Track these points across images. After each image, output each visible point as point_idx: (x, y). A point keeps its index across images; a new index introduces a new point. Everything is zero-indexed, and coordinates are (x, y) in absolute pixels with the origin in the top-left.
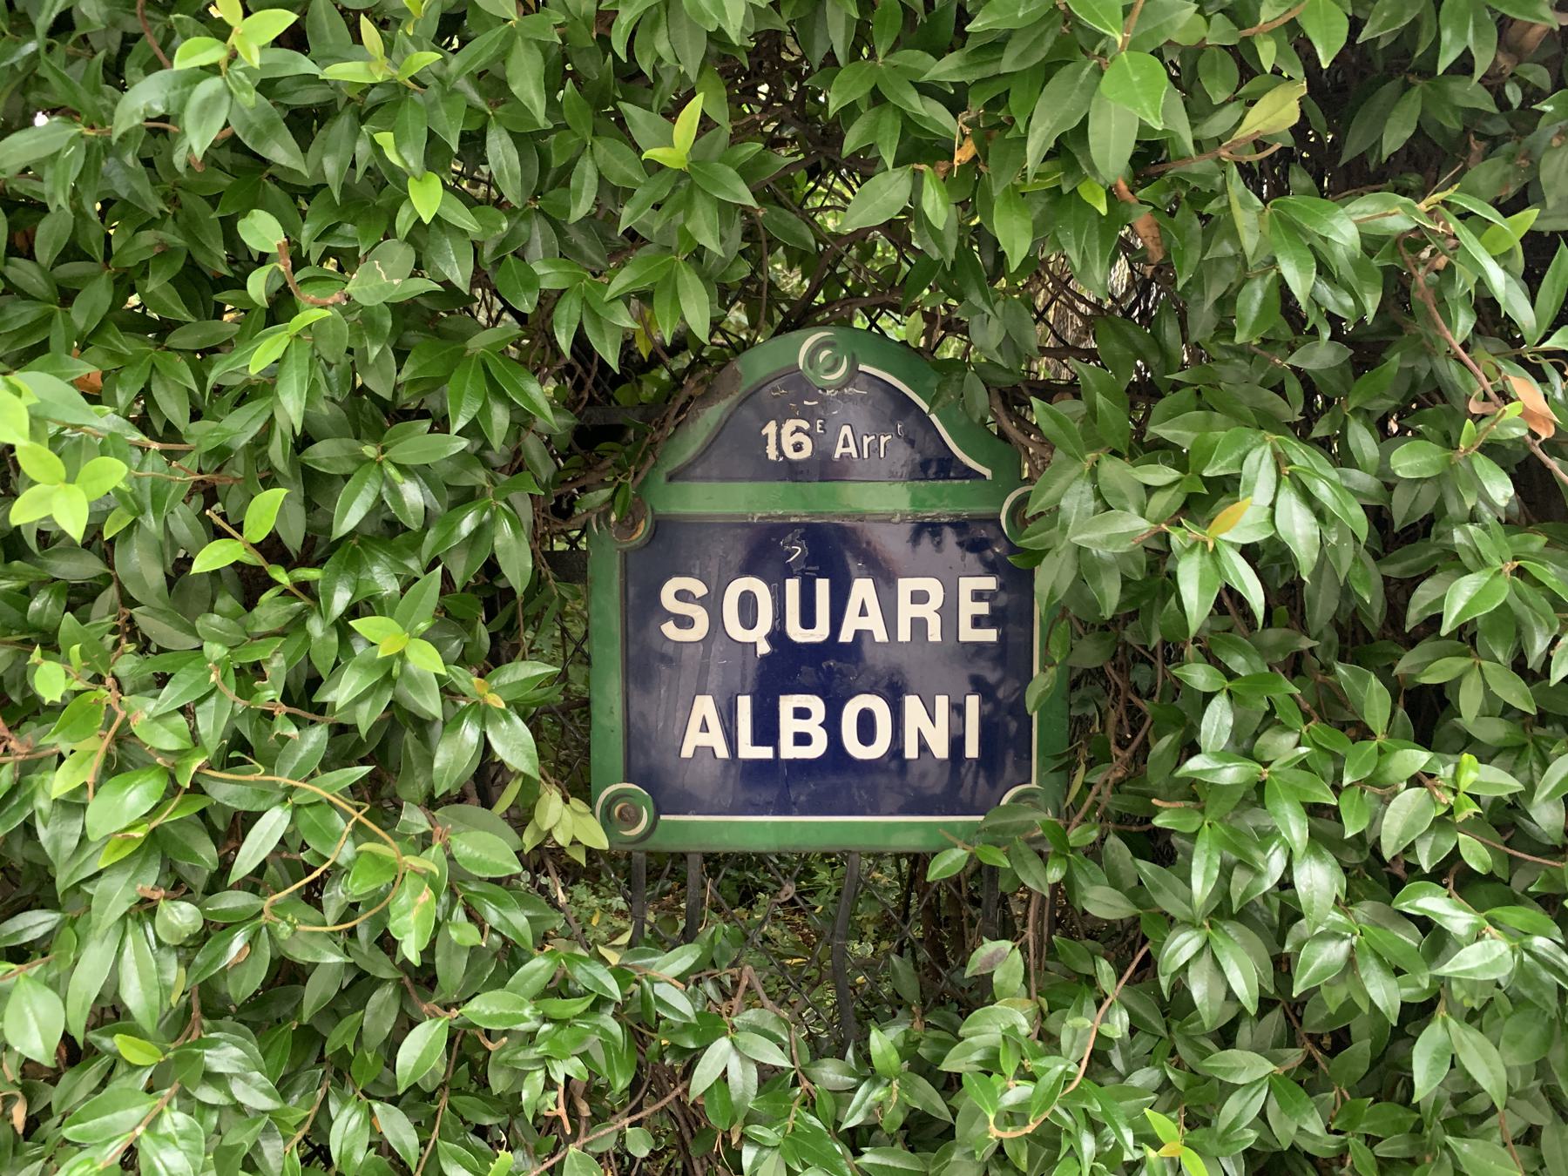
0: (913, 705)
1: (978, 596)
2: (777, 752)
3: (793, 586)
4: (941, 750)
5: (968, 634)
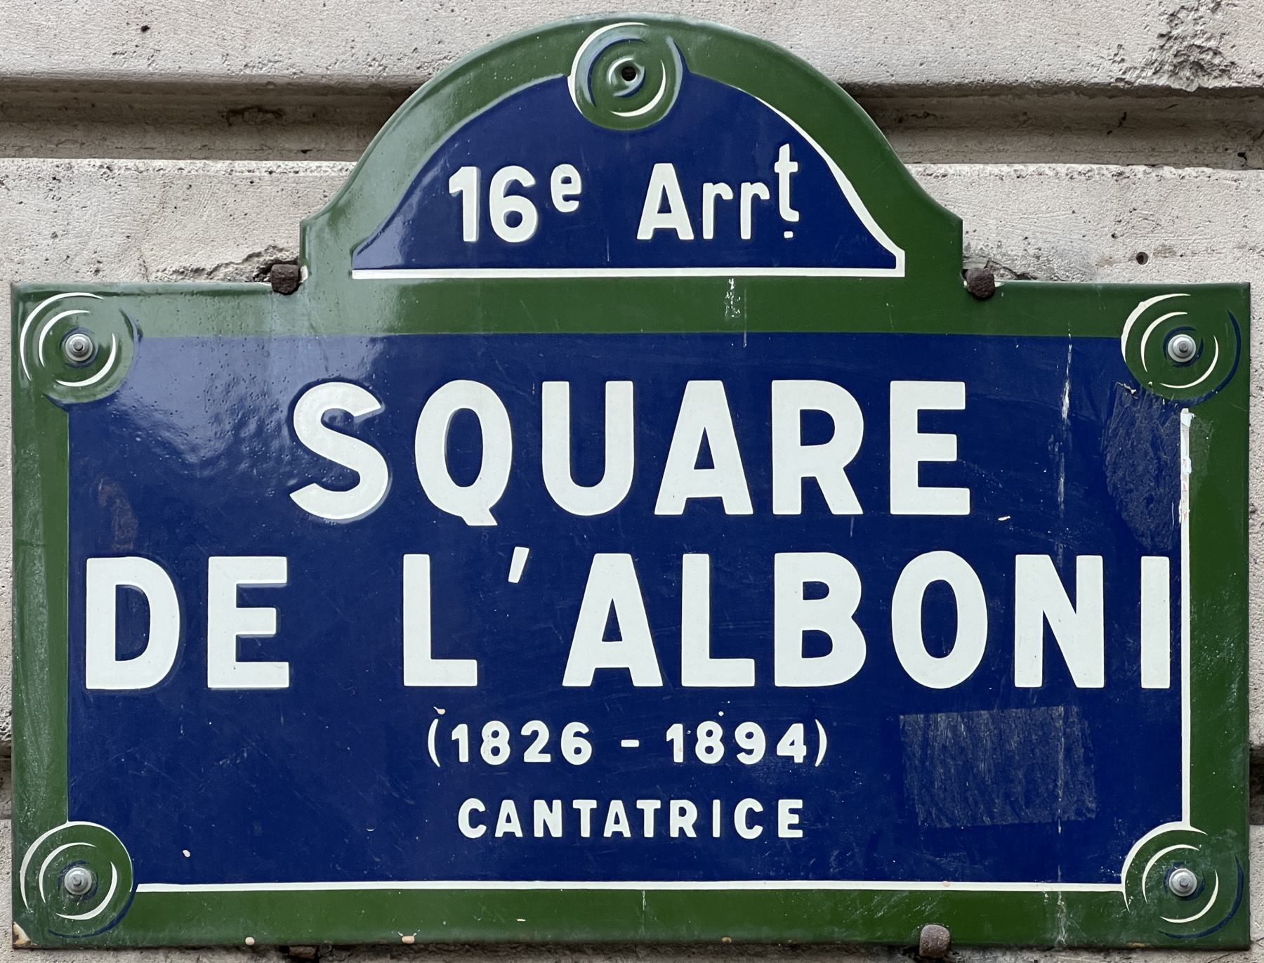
0: (1034, 574)
2: (765, 669)
3: (556, 399)
4: (1088, 672)
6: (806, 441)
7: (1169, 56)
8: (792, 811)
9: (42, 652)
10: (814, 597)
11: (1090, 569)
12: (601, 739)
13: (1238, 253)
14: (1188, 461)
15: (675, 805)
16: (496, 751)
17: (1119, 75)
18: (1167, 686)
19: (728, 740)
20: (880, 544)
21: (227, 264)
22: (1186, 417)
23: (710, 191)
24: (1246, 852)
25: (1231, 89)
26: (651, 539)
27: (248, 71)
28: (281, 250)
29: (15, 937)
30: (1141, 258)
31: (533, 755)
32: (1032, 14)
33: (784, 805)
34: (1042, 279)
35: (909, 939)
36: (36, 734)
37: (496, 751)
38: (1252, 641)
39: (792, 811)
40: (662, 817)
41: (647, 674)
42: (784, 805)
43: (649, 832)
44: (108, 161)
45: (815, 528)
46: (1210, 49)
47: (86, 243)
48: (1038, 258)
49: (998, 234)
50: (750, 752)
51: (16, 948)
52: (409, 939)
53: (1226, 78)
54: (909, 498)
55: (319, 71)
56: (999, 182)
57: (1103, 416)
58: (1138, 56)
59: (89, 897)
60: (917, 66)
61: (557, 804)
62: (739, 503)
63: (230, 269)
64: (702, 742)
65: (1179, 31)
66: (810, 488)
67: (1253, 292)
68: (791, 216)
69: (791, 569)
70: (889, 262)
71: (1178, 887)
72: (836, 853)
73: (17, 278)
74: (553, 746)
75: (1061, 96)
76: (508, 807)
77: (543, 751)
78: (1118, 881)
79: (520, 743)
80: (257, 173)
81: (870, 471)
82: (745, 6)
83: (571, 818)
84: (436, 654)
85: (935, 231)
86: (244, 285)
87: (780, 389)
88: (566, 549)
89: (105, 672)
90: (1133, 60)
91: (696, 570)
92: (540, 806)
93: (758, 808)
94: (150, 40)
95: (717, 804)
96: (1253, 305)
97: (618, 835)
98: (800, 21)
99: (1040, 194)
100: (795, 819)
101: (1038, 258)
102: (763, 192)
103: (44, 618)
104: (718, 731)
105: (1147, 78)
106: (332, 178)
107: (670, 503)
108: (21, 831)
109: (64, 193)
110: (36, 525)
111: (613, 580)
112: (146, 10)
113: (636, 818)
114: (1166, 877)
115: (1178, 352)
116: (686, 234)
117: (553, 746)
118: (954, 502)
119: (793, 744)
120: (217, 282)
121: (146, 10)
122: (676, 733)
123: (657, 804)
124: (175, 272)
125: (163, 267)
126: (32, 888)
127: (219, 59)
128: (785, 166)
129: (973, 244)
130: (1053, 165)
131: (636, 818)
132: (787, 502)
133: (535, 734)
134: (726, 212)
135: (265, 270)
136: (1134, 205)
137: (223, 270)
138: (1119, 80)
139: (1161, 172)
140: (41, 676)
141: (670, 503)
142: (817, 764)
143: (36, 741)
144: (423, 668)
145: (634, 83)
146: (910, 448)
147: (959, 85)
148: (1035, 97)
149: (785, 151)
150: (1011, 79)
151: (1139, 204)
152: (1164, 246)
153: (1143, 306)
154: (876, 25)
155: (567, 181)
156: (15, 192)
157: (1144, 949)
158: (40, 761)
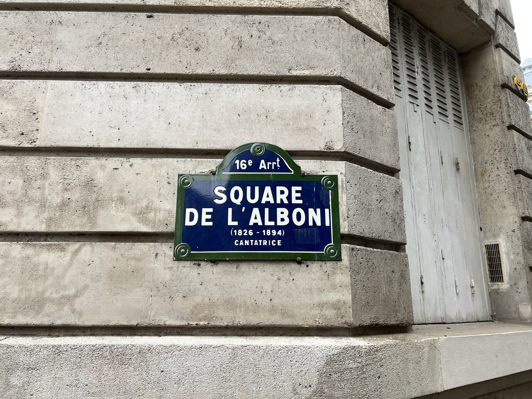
0: (311, 211)
1: (297, 192)
2: (276, 223)
3: (249, 189)
4: (319, 223)
5: (204, 223)
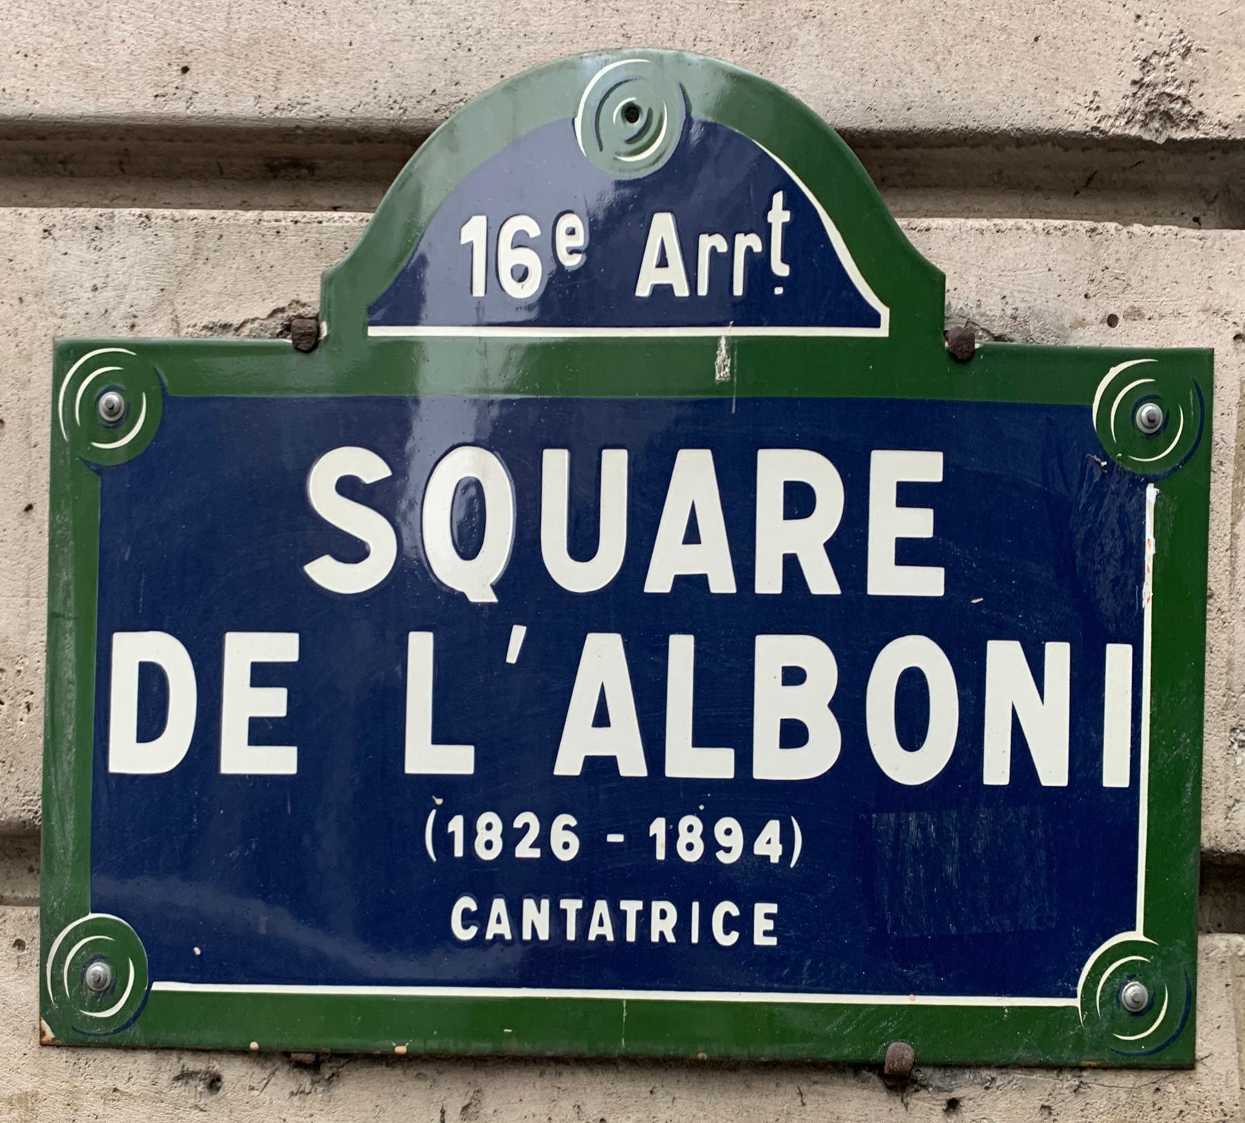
0: (1004, 657)
2: (744, 760)
3: (556, 466)
4: (1053, 769)
6: (788, 516)
7: (1140, 105)
8: (768, 916)
9: (70, 732)
10: (792, 678)
11: (1058, 655)
12: (589, 834)
13: (1203, 317)
14: (1153, 541)
15: (657, 906)
16: (489, 845)
17: (1094, 123)
18: (1127, 785)
19: (708, 836)
20: (855, 624)
21: (254, 320)
22: (1151, 492)
23: (709, 243)
24: (1194, 965)
25: (1199, 141)
26: (635, 613)
27: (278, 114)
28: (304, 305)
29: (43, 1034)
30: (1112, 320)
31: (525, 850)
32: (1014, 57)
33: (761, 909)
34: (1018, 340)
35: (876, 1056)
36: (63, 820)
37: (489, 845)
38: (1206, 737)
39: (768, 916)
40: (644, 918)
41: (633, 765)
42: (761, 909)
43: (631, 936)
44: (146, 211)
45: (794, 610)
46: (1179, 97)
47: (123, 296)
48: (1015, 318)
49: (978, 293)
50: (728, 850)
51: (43, 1045)
52: (401, 1049)
53: (1193, 129)
54: (887, 578)
55: (344, 114)
56: (979, 236)
57: (1074, 490)
58: (1112, 105)
59: (107, 993)
60: (904, 110)
61: (545, 903)
62: (723, 582)
63: (256, 325)
64: (684, 838)
65: (1151, 77)
66: (791, 565)
67: (1216, 359)
68: (781, 269)
69: (772, 652)
70: (874, 321)
71: (1130, 1001)
72: (808, 963)
73: (60, 333)
74: (543, 841)
75: (1038, 148)
76: (499, 906)
77: (533, 846)
78: (1074, 995)
79: (512, 837)
80: (283, 223)
81: (848, 548)
82: (744, 46)
83: (558, 917)
84: (436, 740)
85: (917, 285)
86: (267, 340)
87: (765, 458)
88: (563, 623)
89: (129, 756)
90: (1108, 108)
91: (681, 651)
92: (529, 905)
93: (735, 912)
94: (189, 81)
95: (696, 906)
96: (1216, 373)
97: (601, 938)
98: (795, 61)
99: (1018, 250)
100: (770, 925)
101: (1015, 318)
102: (755, 243)
103: (72, 696)
104: (699, 826)
105: (1118, 128)
106: (353, 229)
107: (658, 581)
108: (48, 922)
109: (105, 244)
110: (68, 596)
111: (603, 660)
112: (187, 49)
113: (619, 919)
114: (1119, 991)
115: (1146, 422)
116: (682, 290)
117: (543, 841)
118: (928, 582)
119: (769, 844)
120: (244, 338)
121: (187, 49)
122: (658, 827)
123: (639, 905)
124: (205, 327)
125: (194, 322)
126: (57, 982)
127: (252, 102)
128: (778, 216)
129: (954, 303)
130: (1030, 221)
131: (619, 919)
132: (769, 581)
133: (526, 826)
134: (721, 263)
135: (288, 328)
136: (1106, 263)
137: (249, 326)
138: (1094, 129)
139: (1131, 229)
140: (69, 758)
141: (658, 581)
142: (792, 865)
143: (63, 825)
144: (427, 756)
145: (639, 123)
146: (891, 523)
147: (944, 132)
148: (1011, 149)
149: (778, 198)
150: (993, 126)
151: (1111, 263)
152: (1133, 307)
153: (1114, 372)
154: (867, 67)
155: (572, 232)
156: (60, 243)
157: (1094, 1068)
158: (65, 849)
